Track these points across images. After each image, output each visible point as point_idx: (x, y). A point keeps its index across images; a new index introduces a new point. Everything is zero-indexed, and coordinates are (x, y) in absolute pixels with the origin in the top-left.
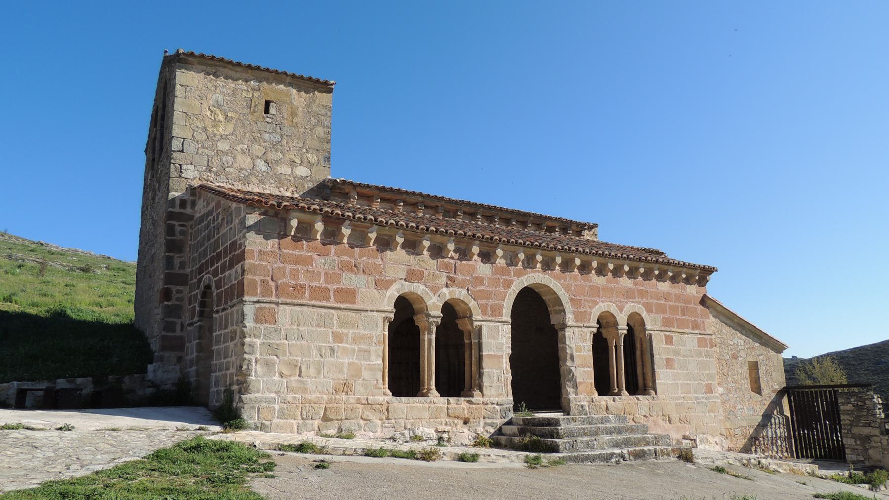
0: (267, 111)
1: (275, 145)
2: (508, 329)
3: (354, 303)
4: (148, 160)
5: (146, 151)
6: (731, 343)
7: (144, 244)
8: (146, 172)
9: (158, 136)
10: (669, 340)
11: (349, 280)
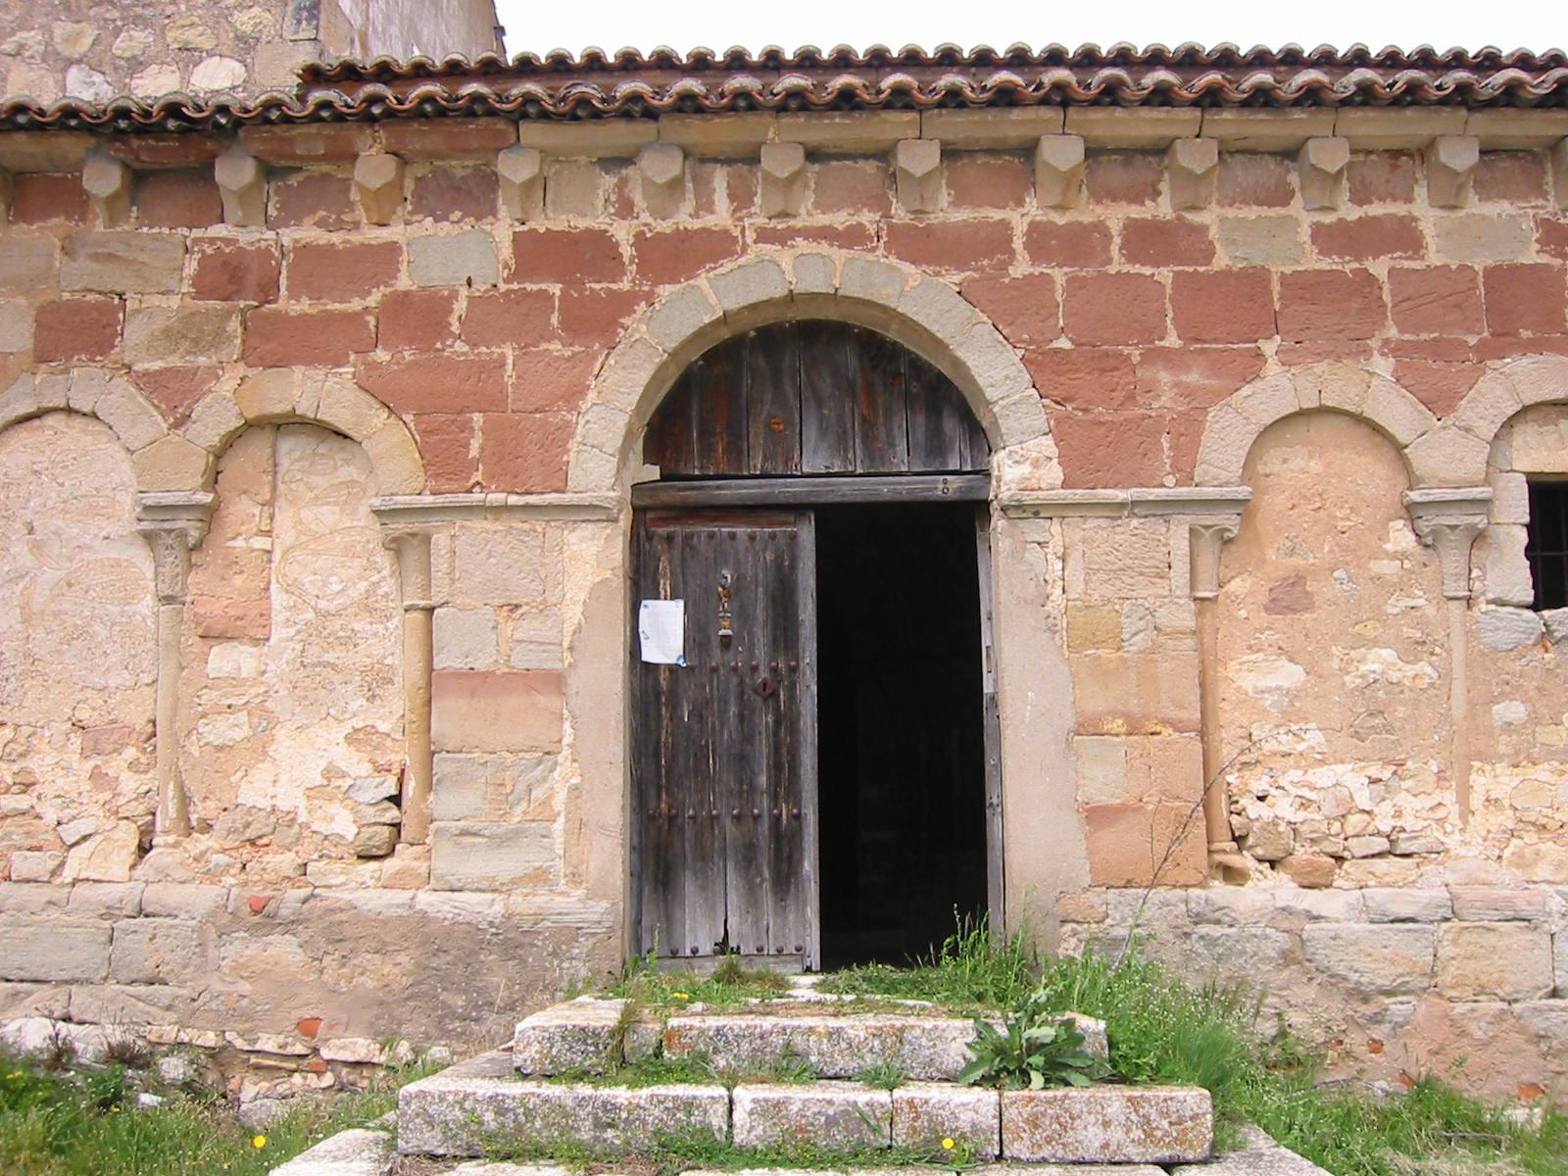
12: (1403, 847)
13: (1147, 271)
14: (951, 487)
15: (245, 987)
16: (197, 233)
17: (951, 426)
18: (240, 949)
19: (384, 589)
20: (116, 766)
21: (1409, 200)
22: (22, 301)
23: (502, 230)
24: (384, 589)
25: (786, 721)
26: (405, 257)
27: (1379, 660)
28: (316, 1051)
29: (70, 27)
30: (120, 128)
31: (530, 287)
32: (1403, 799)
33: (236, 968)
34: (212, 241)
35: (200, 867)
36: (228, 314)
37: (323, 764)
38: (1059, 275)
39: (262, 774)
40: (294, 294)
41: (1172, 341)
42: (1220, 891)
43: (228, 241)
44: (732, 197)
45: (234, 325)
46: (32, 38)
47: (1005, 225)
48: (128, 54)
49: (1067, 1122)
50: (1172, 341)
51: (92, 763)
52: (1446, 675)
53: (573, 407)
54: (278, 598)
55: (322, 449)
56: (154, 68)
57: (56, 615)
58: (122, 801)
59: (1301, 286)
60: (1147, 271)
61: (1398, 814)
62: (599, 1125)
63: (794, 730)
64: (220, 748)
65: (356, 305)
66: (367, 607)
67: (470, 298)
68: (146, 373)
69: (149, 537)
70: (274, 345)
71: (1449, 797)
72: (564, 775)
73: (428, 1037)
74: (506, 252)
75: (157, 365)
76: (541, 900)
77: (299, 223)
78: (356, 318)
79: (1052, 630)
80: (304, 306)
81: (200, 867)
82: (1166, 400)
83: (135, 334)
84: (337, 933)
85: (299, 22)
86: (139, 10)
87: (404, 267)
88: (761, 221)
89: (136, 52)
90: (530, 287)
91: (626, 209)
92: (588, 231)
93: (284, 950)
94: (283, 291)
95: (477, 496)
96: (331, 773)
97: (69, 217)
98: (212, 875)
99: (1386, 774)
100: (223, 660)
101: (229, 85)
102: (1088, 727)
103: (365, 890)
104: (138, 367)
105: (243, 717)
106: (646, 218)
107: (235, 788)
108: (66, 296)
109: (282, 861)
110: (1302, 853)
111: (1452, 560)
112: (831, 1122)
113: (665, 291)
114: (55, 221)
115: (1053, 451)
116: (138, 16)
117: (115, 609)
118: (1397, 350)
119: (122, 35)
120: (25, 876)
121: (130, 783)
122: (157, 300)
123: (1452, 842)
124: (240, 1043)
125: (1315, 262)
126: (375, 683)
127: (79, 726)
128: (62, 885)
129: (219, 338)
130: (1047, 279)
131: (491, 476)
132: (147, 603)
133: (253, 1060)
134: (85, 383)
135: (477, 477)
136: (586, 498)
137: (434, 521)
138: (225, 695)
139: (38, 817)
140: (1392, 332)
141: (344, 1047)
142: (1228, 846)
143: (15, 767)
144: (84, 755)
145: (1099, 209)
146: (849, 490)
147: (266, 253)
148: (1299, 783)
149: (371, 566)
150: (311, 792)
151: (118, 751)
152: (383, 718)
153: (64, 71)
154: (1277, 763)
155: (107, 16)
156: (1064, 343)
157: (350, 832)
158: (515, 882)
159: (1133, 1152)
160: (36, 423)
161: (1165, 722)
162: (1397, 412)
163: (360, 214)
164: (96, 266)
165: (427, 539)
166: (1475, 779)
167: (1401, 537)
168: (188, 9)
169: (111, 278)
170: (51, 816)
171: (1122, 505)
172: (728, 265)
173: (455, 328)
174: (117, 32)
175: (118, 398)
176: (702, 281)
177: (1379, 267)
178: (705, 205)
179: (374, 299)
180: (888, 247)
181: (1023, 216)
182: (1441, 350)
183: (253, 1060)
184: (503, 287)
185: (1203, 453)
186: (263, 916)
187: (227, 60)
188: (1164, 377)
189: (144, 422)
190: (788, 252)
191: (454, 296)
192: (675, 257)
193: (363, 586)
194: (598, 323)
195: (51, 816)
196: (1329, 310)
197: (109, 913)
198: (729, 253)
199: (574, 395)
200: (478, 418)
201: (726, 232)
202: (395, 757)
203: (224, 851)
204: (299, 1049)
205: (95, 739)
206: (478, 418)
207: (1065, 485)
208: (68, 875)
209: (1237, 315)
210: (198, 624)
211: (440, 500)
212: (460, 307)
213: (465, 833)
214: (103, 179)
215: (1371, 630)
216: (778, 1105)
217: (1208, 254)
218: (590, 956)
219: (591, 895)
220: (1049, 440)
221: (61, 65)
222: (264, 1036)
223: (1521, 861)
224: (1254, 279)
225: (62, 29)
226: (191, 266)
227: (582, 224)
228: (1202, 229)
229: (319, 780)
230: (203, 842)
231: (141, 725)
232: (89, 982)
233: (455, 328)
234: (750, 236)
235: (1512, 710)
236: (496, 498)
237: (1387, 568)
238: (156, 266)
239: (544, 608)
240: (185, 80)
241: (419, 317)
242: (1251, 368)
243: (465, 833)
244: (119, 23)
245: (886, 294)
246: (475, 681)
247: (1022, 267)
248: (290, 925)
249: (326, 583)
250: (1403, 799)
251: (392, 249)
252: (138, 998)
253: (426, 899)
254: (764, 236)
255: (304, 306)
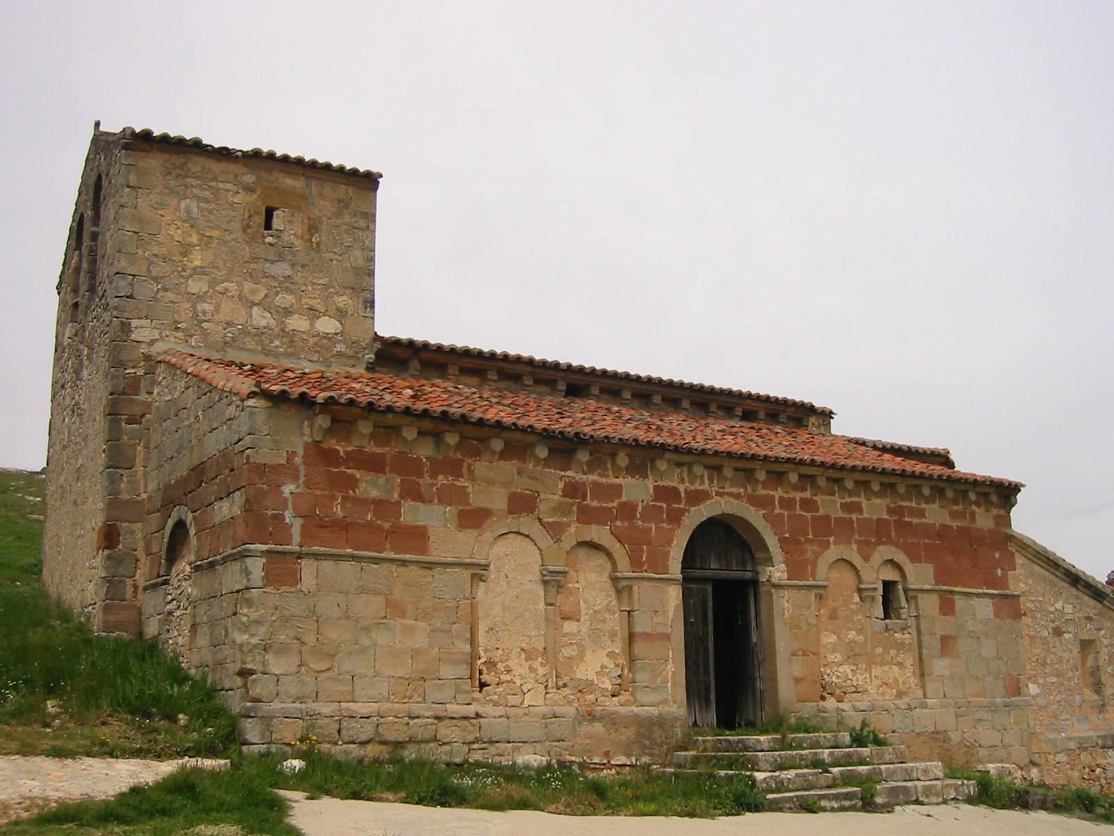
0: (268, 226)
1: (286, 284)
2: (674, 595)
3: (423, 551)
4: (62, 303)
5: (59, 288)
6: (1052, 609)
7: (58, 447)
8: (60, 323)
9: (85, 265)
10: (947, 607)
11: (411, 514)
12: (859, 690)
13: (805, 514)
14: (748, 575)
15: (588, 741)
16: (563, 473)
17: (747, 556)
18: (585, 728)
19: (613, 603)
20: (536, 664)
21: (860, 497)
22: (503, 490)
23: (650, 483)
24: (613, 603)
25: (706, 649)
26: (624, 490)
27: (852, 635)
28: (609, 762)
29: (252, 285)
30: (547, 436)
31: (658, 504)
32: (858, 676)
33: (585, 735)
34: (568, 477)
35: (566, 700)
36: (572, 505)
37: (600, 664)
38: (786, 513)
39: (582, 667)
40: (592, 499)
41: (811, 536)
42: (822, 703)
43: (573, 478)
44: (709, 479)
45: (575, 508)
46: (232, 286)
47: (773, 496)
48: (282, 306)
49: (883, 754)
50: (811, 536)
51: (529, 663)
52: (866, 639)
53: (670, 546)
54: (582, 605)
55: (591, 553)
56: (296, 316)
57: (513, 608)
58: (539, 677)
59: (839, 521)
60: (805, 514)
61: (857, 680)
62: (801, 760)
63: (708, 653)
64: (569, 658)
65: (610, 505)
66: (608, 609)
67: (642, 506)
68: (547, 523)
69: (545, 583)
70: (587, 516)
71: (868, 675)
72: (670, 667)
73: (640, 756)
74: (652, 491)
75: (551, 520)
76: (666, 709)
77: (593, 473)
78: (610, 509)
79: (786, 624)
80: (595, 504)
81: (566, 700)
82: (809, 554)
83: (543, 508)
84: (613, 721)
85: (366, 308)
86: (288, 284)
87: (624, 493)
88: (716, 488)
89: (288, 306)
90: (658, 504)
91: (682, 481)
92: (673, 487)
93: (598, 727)
94: (589, 498)
95: (646, 574)
96: (603, 667)
97: (520, 461)
98: (570, 703)
99: (854, 669)
100: (569, 627)
101: (334, 331)
102: (794, 654)
103: (612, 705)
104: (546, 520)
105: (575, 646)
106: (688, 484)
107: (574, 672)
108: (519, 490)
109: (591, 697)
110: (838, 691)
111: (868, 604)
112: (843, 756)
113: (693, 509)
114: (514, 462)
115: (785, 569)
116: (287, 288)
117: (532, 607)
118: (858, 542)
119: (280, 295)
120: (513, 704)
121: (541, 671)
122: (551, 496)
123: (869, 688)
124: (588, 761)
125: (841, 514)
126: (613, 635)
127: (523, 650)
128: (525, 708)
129: (569, 513)
130: (783, 514)
131: (649, 568)
132: (542, 605)
133: (592, 766)
134: (526, 523)
135: (645, 568)
136: (672, 577)
137: (635, 582)
138: (569, 639)
139: (514, 683)
140: (856, 537)
141: (618, 760)
142: (825, 690)
143: (504, 665)
144: (527, 660)
145: (794, 493)
146: (724, 574)
147: (584, 484)
148: (840, 672)
149: (608, 595)
150: (598, 673)
151: (536, 659)
152: (616, 648)
153: (251, 308)
154: (832, 665)
155: (272, 284)
156: (787, 535)
157: (610, 687)
158: (660, 703)
159: (895, 761)
160: (506, 536)
161: (811, 653)
162: (857, 561)
163: (610, 473)
164: (529, 481)
165: (631, 588)
166: (873, 670)
167: (856, 599)
168: (313, 289)
169: (534, 485)
170: (518, 683)
171: (801, 586)
172: (708, 502)
173: (638, 516)
174: (277, 294)
175: (536, 530)
176: (701, 507)
177: (854, 517)
178: (702, 482)
179: (615, 504)
180: (747, 500)
181: (778, 493)
182: (867, 543)
183: (592, 766)
184: (651, 503)
185: (817, 572)
186: (591, 717)
187: (332, 319)
188: (809, 548)
189: (545, 541)
190: (723, 502)
191: (638, 505)
192: (697, 498)
193: (606, 602)
194: (675, 518)
195: (518, 683)
196: (843, 529)
197: (544, 717)
198: (708, 499)
199: (670, 542)
200: (645, 547)
201: (708, 491)
202: (620, 661)
203: (573, 694)
204: (605, 761)
205: (529, 654)
206: (645, 547)
207: (788, 579)
208: (526, 704)
209: (825, 527)
210: (561, 614)
211: (634, 574)
212: (640, 509)
213: (646, 687)
214: (542, 452)
215: (850, 625)
216: (833, 752)
217: (818, 511)
218: (681, 726)
219: (679, 707)
220: (784, 565)
221: (249, 305)
222: (595, 758)
223: (883, 694)
224: (827, 517)
225: (248, 286)
226: (561, 485)
227: (672, 484)
228: (816, 502)
229: (599, 670)
230: (566, 691)
231: (541, 649)
232: (541, 742)
233: (638, 516)
234: (714, 494)
235: (879, 650)
236: (651, 575)
237: (853, 607)
238: (551, 485)
239: (664, 613)
240: (312, 325)
241: (627, 510)
242: (826, 546)
243: (646, 687)
244: (278, 289)
245: (746, 516)
246: (648, 636)
247: (777, 511)
248: (600, 719)
249: (596, 600)
250: (858, 676)
251: (620, 486)
252: (556, 747)
253: (636, 709)
254: (718, 494)
255: (595, 504)
